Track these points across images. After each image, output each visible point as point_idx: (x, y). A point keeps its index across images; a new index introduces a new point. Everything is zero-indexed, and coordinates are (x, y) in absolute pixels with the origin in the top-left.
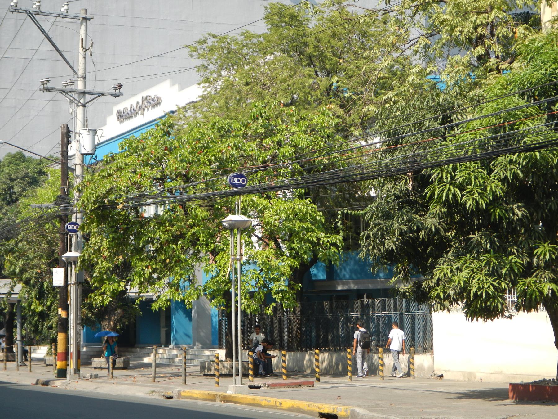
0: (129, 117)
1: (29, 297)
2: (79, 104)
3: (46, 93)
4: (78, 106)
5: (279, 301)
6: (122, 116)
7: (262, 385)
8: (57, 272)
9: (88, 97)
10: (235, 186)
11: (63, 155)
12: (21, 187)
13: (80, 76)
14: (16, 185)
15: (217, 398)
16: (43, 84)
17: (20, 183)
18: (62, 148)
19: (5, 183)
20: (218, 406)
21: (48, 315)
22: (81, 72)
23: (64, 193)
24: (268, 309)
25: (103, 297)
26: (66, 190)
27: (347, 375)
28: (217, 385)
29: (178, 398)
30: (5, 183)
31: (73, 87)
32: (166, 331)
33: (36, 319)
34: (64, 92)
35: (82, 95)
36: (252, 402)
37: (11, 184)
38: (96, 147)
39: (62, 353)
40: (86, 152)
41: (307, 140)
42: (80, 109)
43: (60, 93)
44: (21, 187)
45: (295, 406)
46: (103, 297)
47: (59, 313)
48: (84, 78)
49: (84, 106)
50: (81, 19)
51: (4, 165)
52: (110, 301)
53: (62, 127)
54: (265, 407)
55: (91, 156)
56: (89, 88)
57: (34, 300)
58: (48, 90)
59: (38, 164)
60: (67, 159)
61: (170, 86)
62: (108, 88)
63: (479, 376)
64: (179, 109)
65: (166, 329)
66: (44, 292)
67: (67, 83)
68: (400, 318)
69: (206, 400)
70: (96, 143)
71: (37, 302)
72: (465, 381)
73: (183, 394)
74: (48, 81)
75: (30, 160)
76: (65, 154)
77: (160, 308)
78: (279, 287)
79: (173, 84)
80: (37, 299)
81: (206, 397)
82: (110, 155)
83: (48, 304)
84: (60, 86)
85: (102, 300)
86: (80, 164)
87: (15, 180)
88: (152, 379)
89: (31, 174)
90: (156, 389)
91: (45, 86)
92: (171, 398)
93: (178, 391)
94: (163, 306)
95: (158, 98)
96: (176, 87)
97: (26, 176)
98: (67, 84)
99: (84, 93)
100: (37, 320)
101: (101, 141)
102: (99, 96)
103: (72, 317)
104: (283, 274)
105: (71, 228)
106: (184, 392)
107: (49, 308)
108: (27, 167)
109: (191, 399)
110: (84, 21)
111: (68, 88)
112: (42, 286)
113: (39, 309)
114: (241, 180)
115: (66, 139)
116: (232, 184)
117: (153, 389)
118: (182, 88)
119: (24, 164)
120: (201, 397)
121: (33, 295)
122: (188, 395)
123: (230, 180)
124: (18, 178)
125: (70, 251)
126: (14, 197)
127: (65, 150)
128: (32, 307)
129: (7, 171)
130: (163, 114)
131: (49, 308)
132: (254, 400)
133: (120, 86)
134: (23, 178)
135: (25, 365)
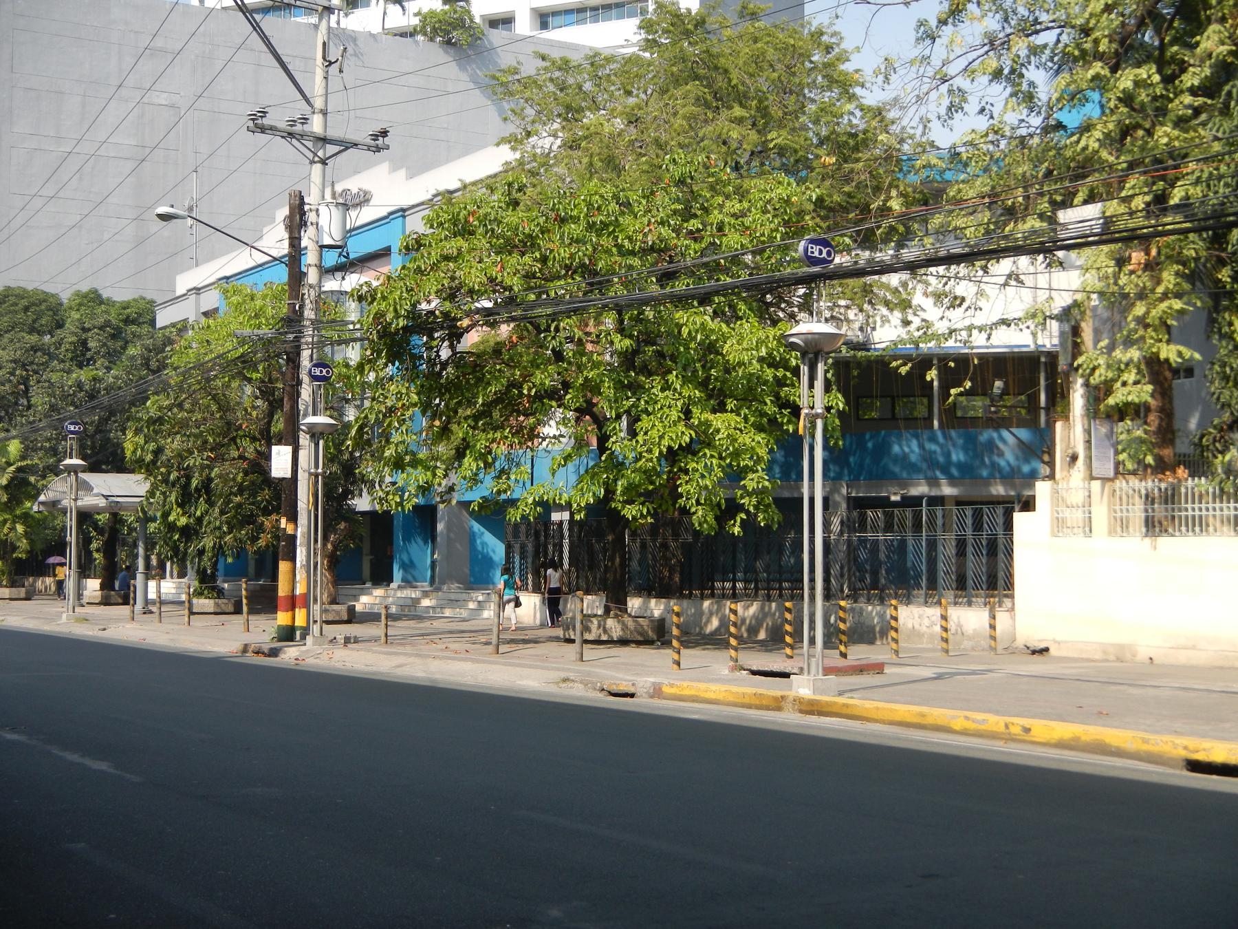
4: (312, 162)
5: (751, 509)
7: (795, 671)
8: (278, 453)
10: (813, 261)
11: (292, 245)
15: (788, 706)
18: (291, 233)
19: (75, 334)
20: (790, 719)
21: (197, 533)
22: (318, 103)
23: (294, 311)
24: (734, 525)
25: (402, 497)
27: (783, 641)
28: (676, 666)
29: (652, 697)
30: (75, 334)
33: (176, 537)
34: (291, 135)
35: (320, 144)
36: (915, 720)
37: (84, 336)
38: (349, 233)
40: (332, 242)
42: (319, 166)
45: (1084, 738)
46: (402, 497)
47: (283, 526)
49: (324, 162)
50: (320, 9)
51: (71, 308)
54: (964, 733)
56: (331, 133)
58: (263, 129)
59: (124, 308)
62: (363, 136)
63: (1143, 654)
64: (465, 187)
66: (190, 494)
68: (928, 545)
69: (743, 706)
72: (1107, 661)
73: (666, 689)
75: (109, 303)
78: (758, 482)
79: (394, 169)
80: (179, 505)
81: (747, 700)
83: (198, 513)
87: (89, 330)
88: (490, 648)
90: (572, 675)
91: (259, 121)
92: (632, 696)
93: (654, 684)
95: (366, 193)
96: (402, 173)
97: (107, 324)
98: (293, 123)
99: (324, 140)
101: (358, 223)
102: (347, 148)
106: (672, 686)
109: (693, 701)
110: (326, 13)
111: (298, 128)
113: (183, 521)
114: (825, 251)
116: (809, 258)
117: (563, 675)
118: (411, 176)
120: (731, 699)
121: (173, 498)
123: (806, 250)
125: (314, 414)
126: (89, 355)
128: (171, 518)
129: (78, 316)
130: (458, 185)
131: (199, 520)
132: (923, 715)
133: (384, 133)
135: (151, 612)
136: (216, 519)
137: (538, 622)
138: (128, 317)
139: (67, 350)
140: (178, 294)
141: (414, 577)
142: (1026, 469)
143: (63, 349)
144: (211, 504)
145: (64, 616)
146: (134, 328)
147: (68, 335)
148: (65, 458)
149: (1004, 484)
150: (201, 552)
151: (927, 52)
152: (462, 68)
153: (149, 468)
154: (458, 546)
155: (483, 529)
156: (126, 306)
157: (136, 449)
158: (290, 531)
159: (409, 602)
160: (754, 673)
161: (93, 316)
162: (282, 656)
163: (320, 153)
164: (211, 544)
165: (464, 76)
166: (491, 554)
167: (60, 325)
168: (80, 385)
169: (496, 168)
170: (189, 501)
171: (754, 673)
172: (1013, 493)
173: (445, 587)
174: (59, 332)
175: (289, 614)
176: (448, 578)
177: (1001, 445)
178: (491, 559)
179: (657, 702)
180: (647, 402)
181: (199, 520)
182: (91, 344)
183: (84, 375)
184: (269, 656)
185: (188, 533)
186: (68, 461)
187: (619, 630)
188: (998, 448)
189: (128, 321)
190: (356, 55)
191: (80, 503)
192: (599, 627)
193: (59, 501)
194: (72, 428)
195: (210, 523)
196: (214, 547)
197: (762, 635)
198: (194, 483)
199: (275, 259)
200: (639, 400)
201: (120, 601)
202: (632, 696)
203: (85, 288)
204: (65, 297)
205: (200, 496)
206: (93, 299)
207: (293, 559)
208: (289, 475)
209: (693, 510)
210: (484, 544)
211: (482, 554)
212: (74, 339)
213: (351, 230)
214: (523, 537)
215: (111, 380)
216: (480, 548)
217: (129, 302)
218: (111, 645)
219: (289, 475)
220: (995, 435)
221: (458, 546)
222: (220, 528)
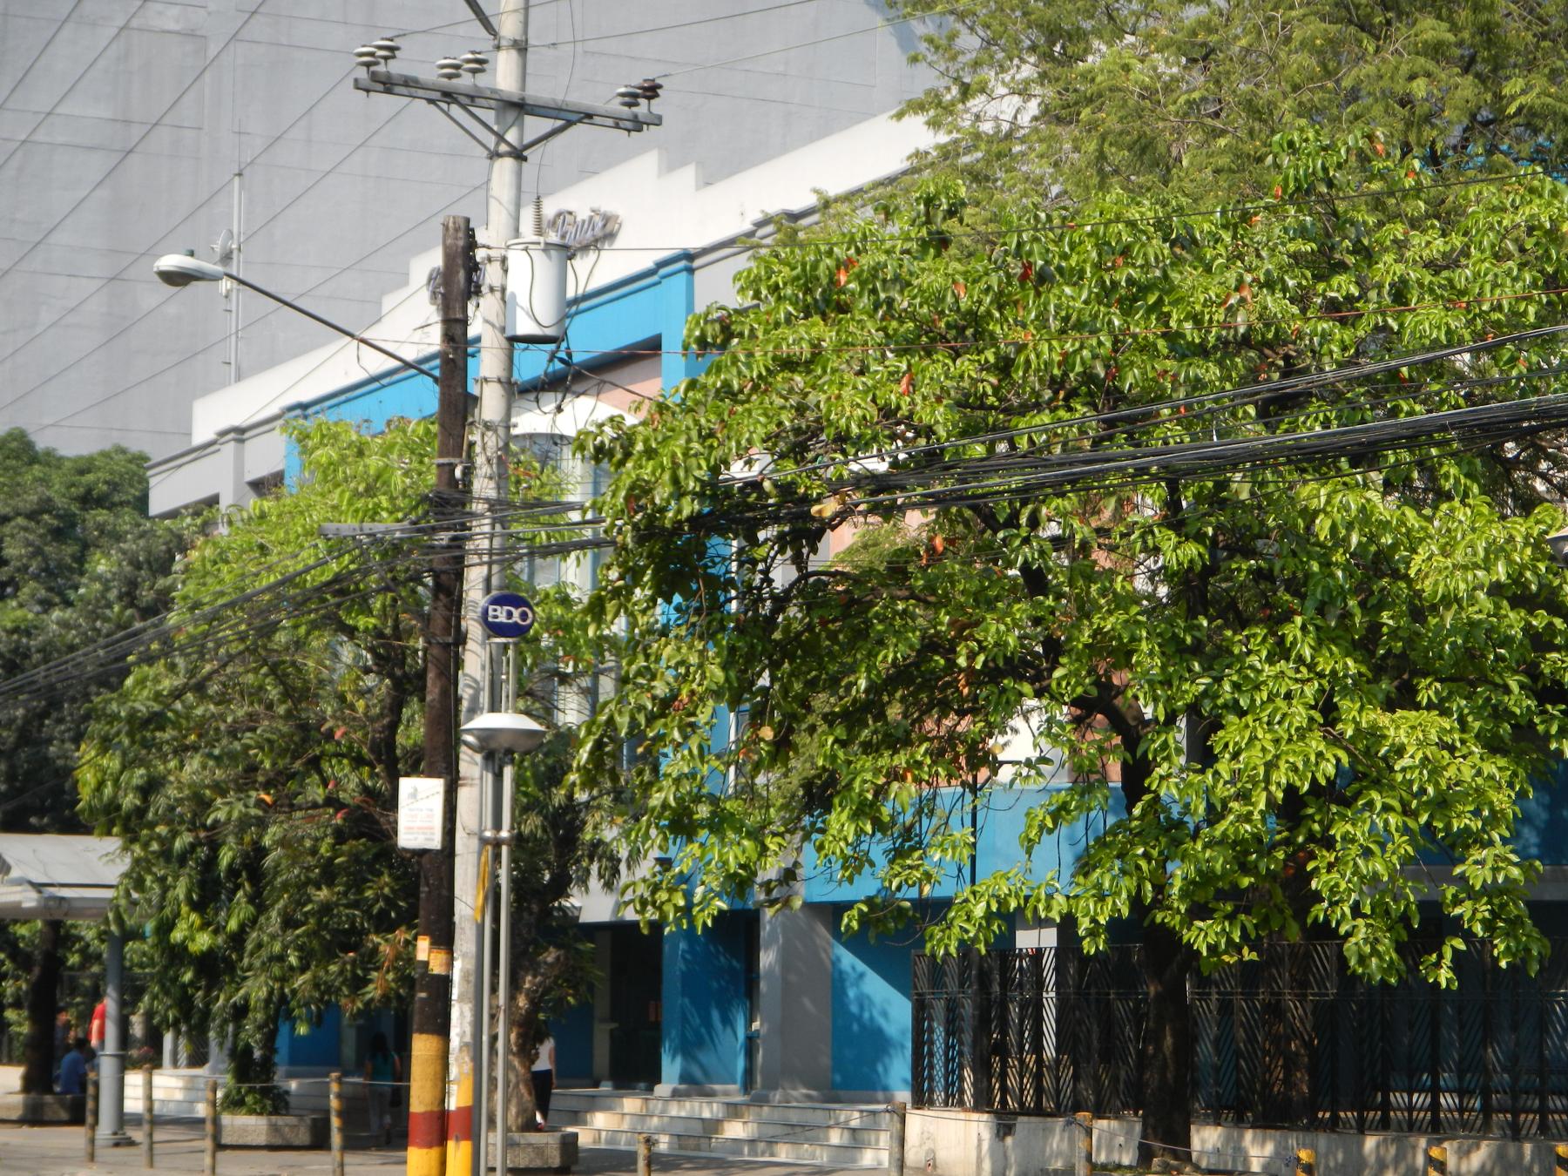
1: (163, 897)
2: (503, 148)
3: (381, 100)
4: (494, 155)
5: (1478, 929)
8: (414, 795)
9: (535, 126)
11: (448, 337)
12: (28, 544)
13: (504, 43)
14: (12, 536)
16: (368, 65)
17: (26, 529)
21: (231, 967)
22: (509, 27)
23: (453, 482)
24: (1438, 965)
25: (688, 895)
26: (458, 473)
31: (482, 81)
32: (612, 1031)
33: (188, 976)
35: (511, 115)
38: (571, 307)
39: (427, 1115)
41: (1515, 279)
42: (508, 163)
43: (431, 101)
44: (28, 544)
48: (521, 47)
49: (519, 155)
52: (721, 911)
53: (446, 227)
55: (552, 347)
56: (538, 91)
57: (185, 909)
58: (388, 85)
59: (82, 472)
60: (466, 355)
61: (660, 174)
62: (604, 95)
65: (614, 1025)
66: (217, 881)
67: (457, 67)
70: (570, 294)
71: (194, 916)
74: (392, 49)
75: (50, 460)
76: (458, 330)
77: (965, 947)
82: (715, 315)
83: (233, 925)
84: (429, 73)
85: (687, 910)
86: (499, 381)
89: (60, 502)
91: (381, 68)
94: (975, 940)
95: (607, 219)
96: (688, 174)
97: (46, 506)
99: (519, 107)
100: (191, 983)
101: (595, 284)
103: (460, 970)
104: (1495, 818)
105: (503, 619)
107: (238, 939)
108: (44, 481)
111: (465, 81)
112: (213, 860)
113: (203, 941)
115: (462, 275)
119: (37, 470)
121: (180, 891)
124: (19, 514)
125: (494, 707)
127: (459, 316)
128: (177, 936)
130: (811, 200)
131: (238, 939)
133: (651, 91)
134: (32, 516)
136: (273, 937)
138: (89, 491)
140: (199, 438)
150: (241, 1011)
154: (807, 1003)
155: (861, 966)
156: (85, 467)
158: (437, 968)
159: (697, 1129)
164: (263, 993)
166: (881, 1021)
169: (894, 163)
173: (777, 1096)
175: (434, 1153)
180: (1236, 687)
189: (88, 500)
195: (260, 946)
196: (268, 1001)
198: (226, 857)
199: (407, 365)
200: (1218, 680)
201: (64, 1115)
205: (238, 887)
207: (443, 1030)
210: (864, 1000)
216: (854, 1009)
217: (91, 459)
221: (807, 1003)
222: (281, 958)
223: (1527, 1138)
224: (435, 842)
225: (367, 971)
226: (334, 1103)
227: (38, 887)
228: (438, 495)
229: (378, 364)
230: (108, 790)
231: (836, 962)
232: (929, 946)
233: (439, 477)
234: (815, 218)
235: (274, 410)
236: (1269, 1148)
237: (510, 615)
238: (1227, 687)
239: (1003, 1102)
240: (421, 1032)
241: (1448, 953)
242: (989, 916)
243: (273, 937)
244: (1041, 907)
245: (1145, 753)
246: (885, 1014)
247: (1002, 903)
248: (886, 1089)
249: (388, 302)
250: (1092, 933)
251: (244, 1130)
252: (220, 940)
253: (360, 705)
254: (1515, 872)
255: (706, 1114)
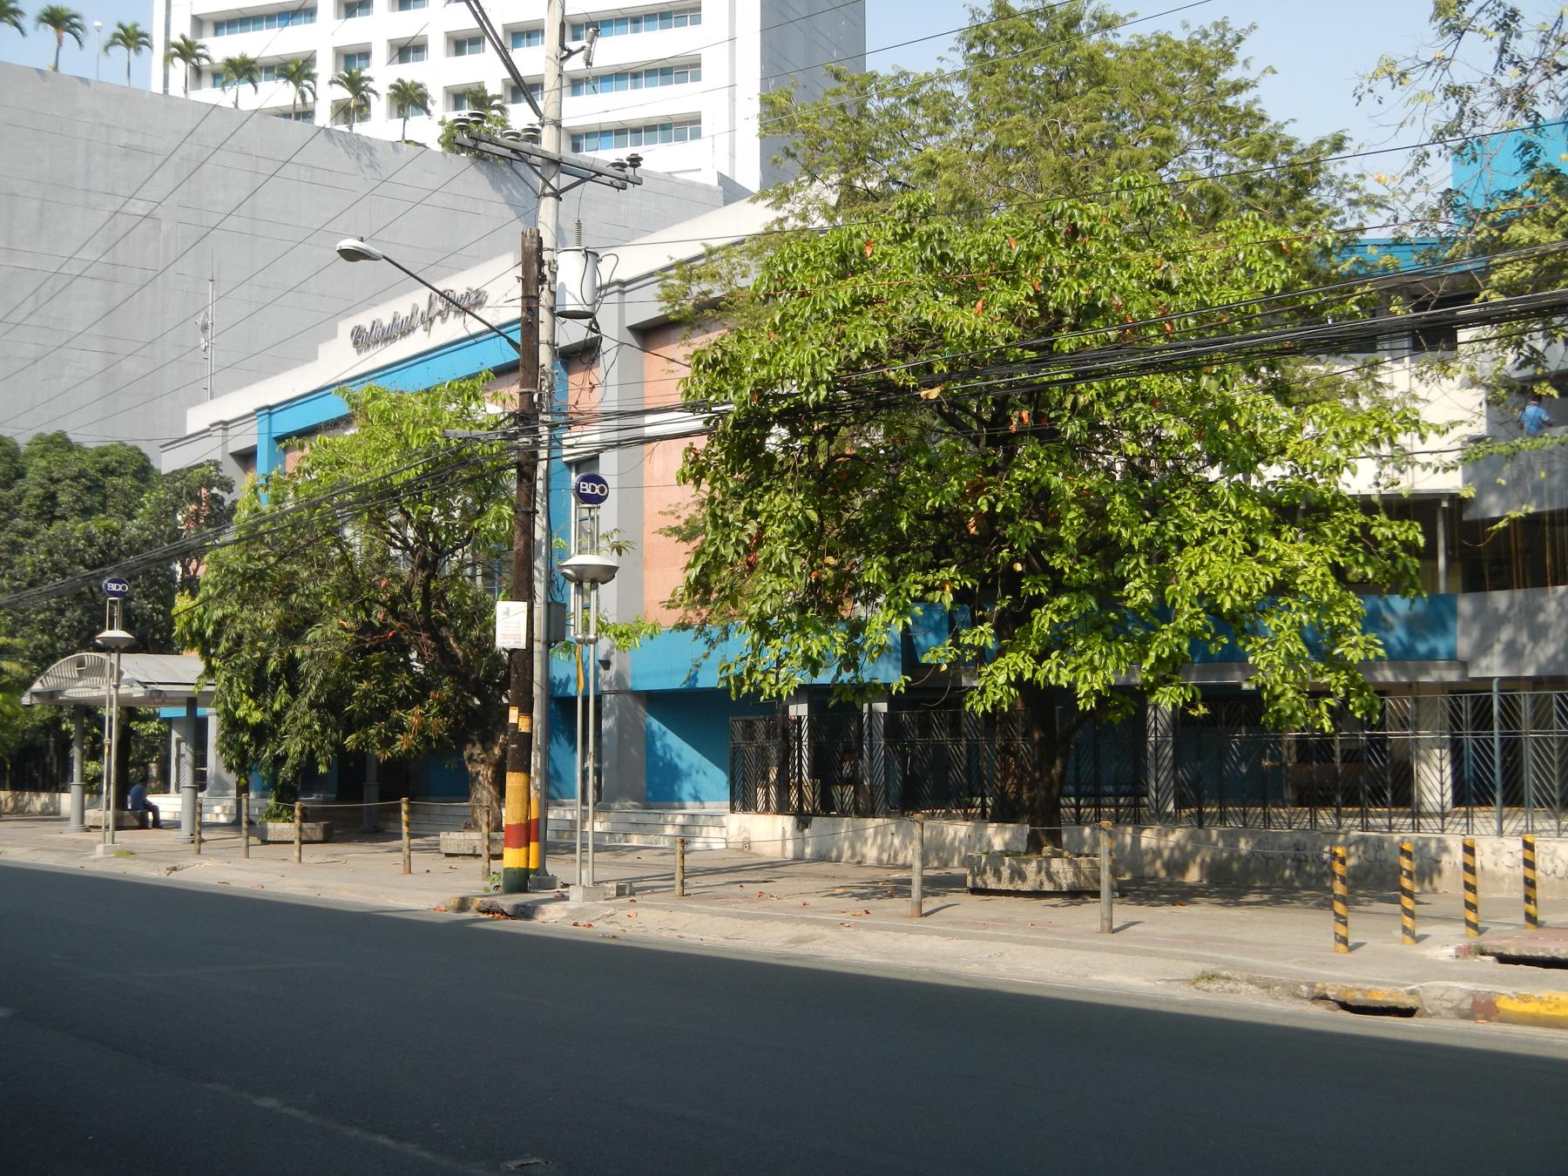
0: (387, 339)
6: (361, 340)
8: (507, 613)
9: (566, 180)
12: (73, 495)
18: (525, 288)
21: (273, 733)
26: (535, 398)
30: (41, 486)
33: (246, 739)
35: (553, 169)
37: (52, 488)
42: (551, 200)
44: (73, 495)
49: (557, 195)
51: (33, 454)
73: (1504, 1004)
75: (80, 448)
83: (277, 706)
87: (59, 481)
89: (92, 472)
92: (1409, 1012)
93: (1473, 994)
97: (82, 474)
102: (583, 180)
105: (589, 491)
113: (256, 717)
122: (1543, 1010)
125: (111, 628)
129: (43, 463)
131: (278, 717)
134: (74, 479)
136: (305, 714)
137: (790, 854)
138: (107, 466)
139: (30, 506)
140: (189, 432)
141: (559, 791)
142: (1422, 648)
143: (24, 504)
144: (294, 691)
145: (100, 848)
146: (116, 481)
147: (31, 487)
148: (103, 629)
149: (1392, 668)
150: (279, 761)
151: (1448, 54)
152: (497, 188)
153: (202, 643)
154: (633, 751)
155: (664, 728)
156: (103, 453)
157: (191, 620)
158: (523, 728)
159: (567, 826)
160: (1504, 959)
161: (63, 463)
162: (540, 918)
163: (553, 182)
164: (299, 748)
165: (498, 198)
166: (677, 760)
167: (21, 474)
168: (90, 540)
169: (758, 229)
170: (265, 688)
171: (1504, 959)
172: (1404, 680)
173: (616, 806)
174: (20, 482)
175: (523, 851)
176: (620, 793)
177: (1390, 618)
178: (676, 766)
179: (1481, 1027)
180: (1178, 527)
181: (278, 717)
182: (62, 498)
183: (94, 526)
184: (514, 917)
185: (261, 733)
186: (107, 633)
187: (1070, 875)
188: (1385, 620)
189: (107, 471)
190: (371, 166)
191: (121, 691)
192: (1039, 871)
193: (61, 692)
194: (113, 587)
195: (295, 719)
196: (302, 753)
197: (1193, 875)
198: (272, 665)
199: (492, 329)
200: (1164, 523)
201: (136, 823)
202: (1409, 1012)
203: (49, 431)
204: (23, 440)
205: (279, 684)
206: (59, 443)
207: (526, 770)
208: (522, 645)
209: (1278, 690)
210: (666, 747)
211: (662, 759)
212: (40, 491)
213: (601, 288)
214: (761, 738)
215: (134, 531)
216: (660, 753)
217: (107, 448)
218: (295, 906)
219: (522, 645)
220: (1381, 603)
221: (633, 751)
222: (309, 726)
223: (1087, 824)
224: (521, 644)
225: (394, 733)
226: (404, 817)
227: (145, 684)
228: (523, 412)
229: (476, 327)
230: (195, 624)
231: (648, 726)
232: (968, 705)
233: (521, 401)
234: (702, 261)
235: (251, 410)
236: (1007, 836)
237: (593, 489)
238: (1171, 527)
239: (800, 806)
240: (513, 771)
241: (1324, 708)
242: (1009, 682)
243: (305, 714)
244: (1051, 676)
245: (1121, 572)
246: (679, 757)
247: (1020, 676)
248: (680, 800)
249: (322, 348)
250: (1087, 695)
251: (282, 831)
252: (267, 716)
253: (493, 545)
254: (1381, 652)
255: (569, 817)
